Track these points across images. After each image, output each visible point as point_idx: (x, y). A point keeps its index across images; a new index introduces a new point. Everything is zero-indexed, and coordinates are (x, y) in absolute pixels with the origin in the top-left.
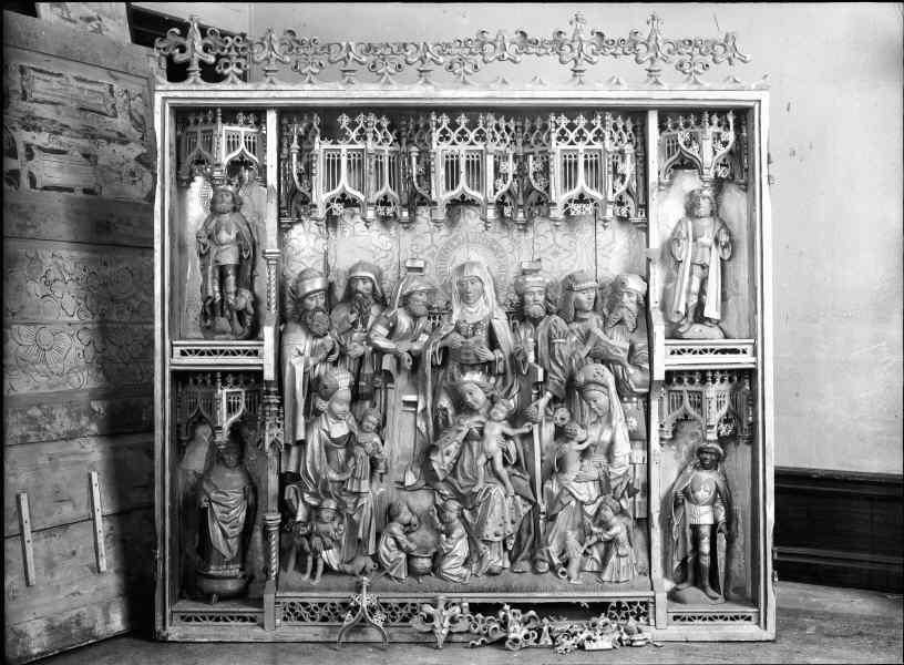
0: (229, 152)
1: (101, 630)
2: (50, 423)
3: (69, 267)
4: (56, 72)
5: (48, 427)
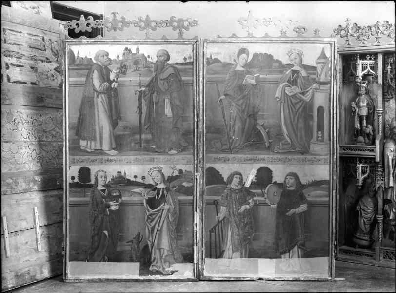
0: (363, 70)
1: (39, 277)
2: (16, 186)
3: (25, 117)
4: (19, 31)
5: (15, 187)
